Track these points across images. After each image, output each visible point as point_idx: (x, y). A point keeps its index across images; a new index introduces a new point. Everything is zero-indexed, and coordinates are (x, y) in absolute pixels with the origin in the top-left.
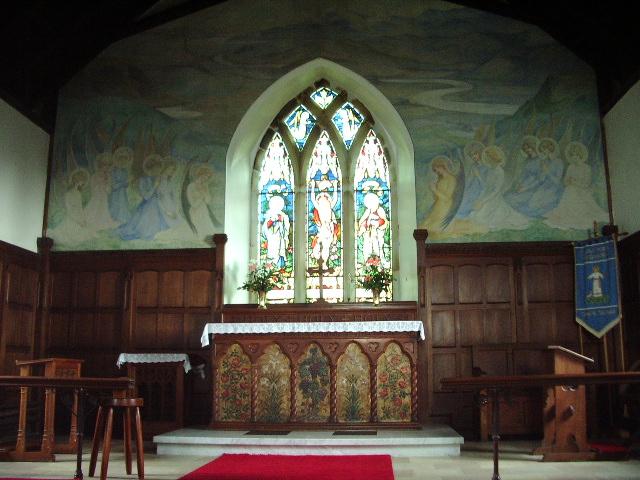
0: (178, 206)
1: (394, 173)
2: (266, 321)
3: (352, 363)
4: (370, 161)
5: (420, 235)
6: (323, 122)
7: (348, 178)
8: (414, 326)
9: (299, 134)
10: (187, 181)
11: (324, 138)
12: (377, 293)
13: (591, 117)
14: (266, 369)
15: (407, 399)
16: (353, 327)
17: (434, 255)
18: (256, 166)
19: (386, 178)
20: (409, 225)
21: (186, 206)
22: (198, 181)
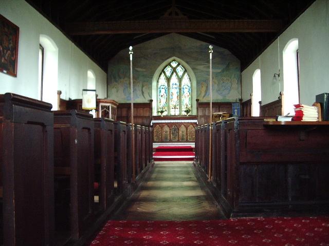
0: (141, 93)
1: (191, 84)
2: (28, 2)
3: (183, 128)
4: (186, 80)
5: (197, 100)
6: (174, 70)
7: (180, 85)
8: (195, 121)
9: (168, 74)
10: (143, 87)
11: (175, 74)
12: (188, 113)
13: (238, 73)
14: (164, 130)
15: (194, 136)
16: (183, 121)
17: (201, 105)
18: (158, 82)
19: (189, 85)
20: (195, 98)
21: (143, 93)
22: (146, 87)
